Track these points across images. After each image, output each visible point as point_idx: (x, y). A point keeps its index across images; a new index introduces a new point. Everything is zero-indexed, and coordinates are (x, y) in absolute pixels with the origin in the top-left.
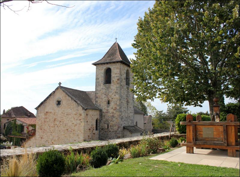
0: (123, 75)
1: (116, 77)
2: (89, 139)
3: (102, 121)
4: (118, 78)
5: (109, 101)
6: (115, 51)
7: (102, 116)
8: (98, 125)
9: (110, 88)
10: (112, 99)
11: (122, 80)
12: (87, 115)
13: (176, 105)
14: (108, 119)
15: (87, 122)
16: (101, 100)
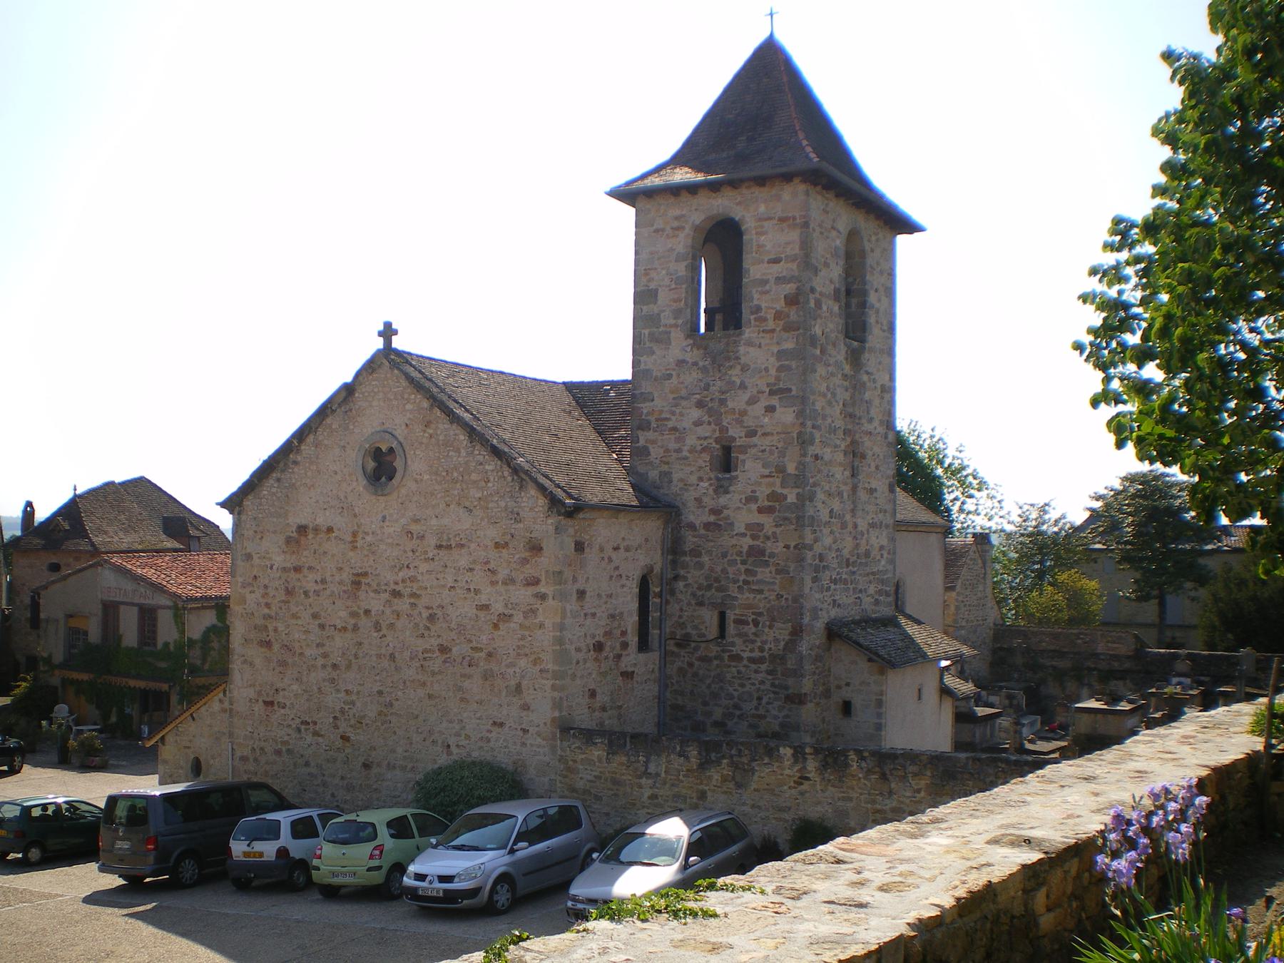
1: (780, 280)
3: (681, 584)
5: (727, 450)
7: (684, 554)
9: (738, 358)
10: (752, 433)
12: (579, 547)
14: (724, 571)
16: (673, 446)
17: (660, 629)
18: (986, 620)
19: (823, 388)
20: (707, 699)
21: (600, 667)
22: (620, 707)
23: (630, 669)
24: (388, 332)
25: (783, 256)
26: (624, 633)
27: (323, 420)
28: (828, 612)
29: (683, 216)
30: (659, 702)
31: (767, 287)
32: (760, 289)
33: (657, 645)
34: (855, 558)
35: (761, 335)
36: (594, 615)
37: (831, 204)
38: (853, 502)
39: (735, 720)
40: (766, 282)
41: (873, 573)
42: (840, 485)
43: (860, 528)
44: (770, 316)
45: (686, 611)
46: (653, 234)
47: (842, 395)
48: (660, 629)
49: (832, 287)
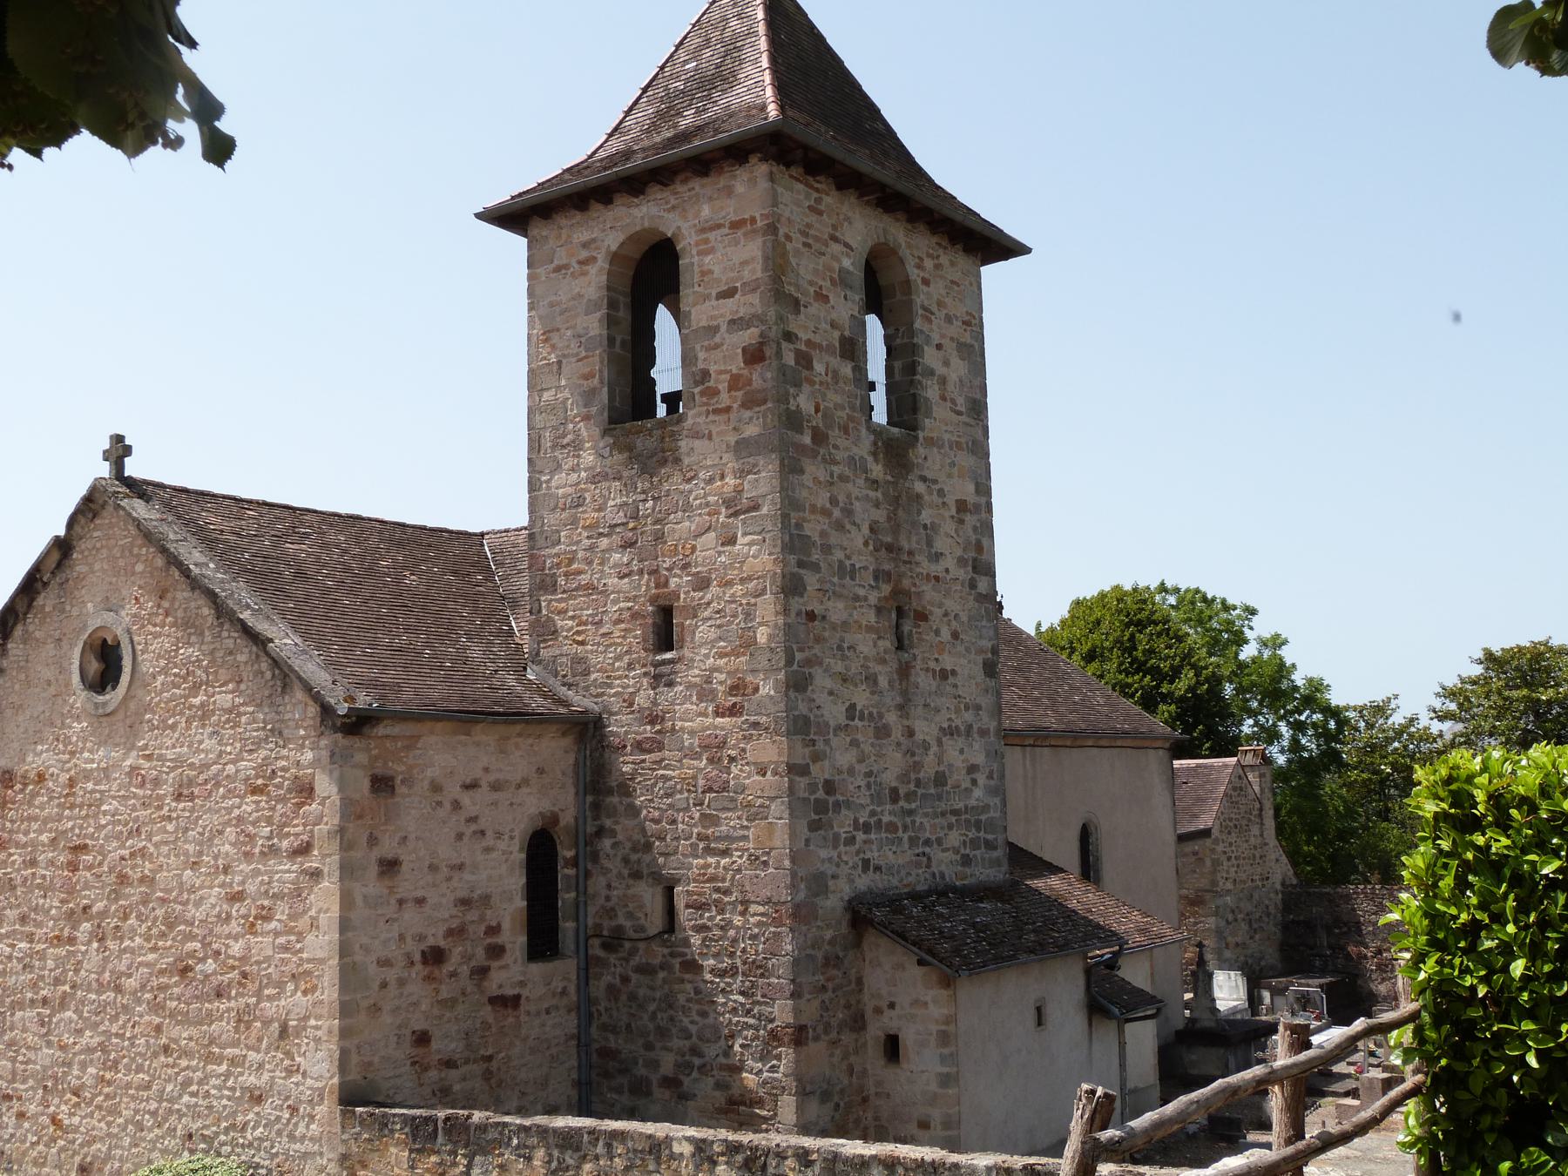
0: (822, 297)
1: (736, 324)
2: (433, 1074)
3: (607, 843)
4: (750, 336)
5: (665, 614)
6: (733, 50)
7: (610, 792)
8: (566, 897)
9: (677, 461)
10: (702, 583)
11: (804, 360)
12: (382, 784)
13: (1490, 986)
15: (390, 866)
17: (577, 920)
18: (1268, 878)
19: (822, 499)
20: (651, 1038)
21: (437, 991)
22: (490, 1058)
23: (510, 992)
24: (119, 450)
25: (738, 285)
26: (494, 930)
27: (33, 600)
28: (851, 881)
29: (594, 240)
30: (578, 1046)
31: (717, 339)
32: (706, 343)
33: (572, 947)
34: (912, 786)
35: (712, 417)
36: (420, 901)
37: (828, 200)
38: (905, 693)
39: (695, 1074)
40: (716, 329)
41: (955, 812)
42: (871, 665)
43: (919, 736)
44: (723, 387)
45: (616, 888)
46: (552, 275)
47: (866, 514)
48: (577, 920)
49: (836, 334)
